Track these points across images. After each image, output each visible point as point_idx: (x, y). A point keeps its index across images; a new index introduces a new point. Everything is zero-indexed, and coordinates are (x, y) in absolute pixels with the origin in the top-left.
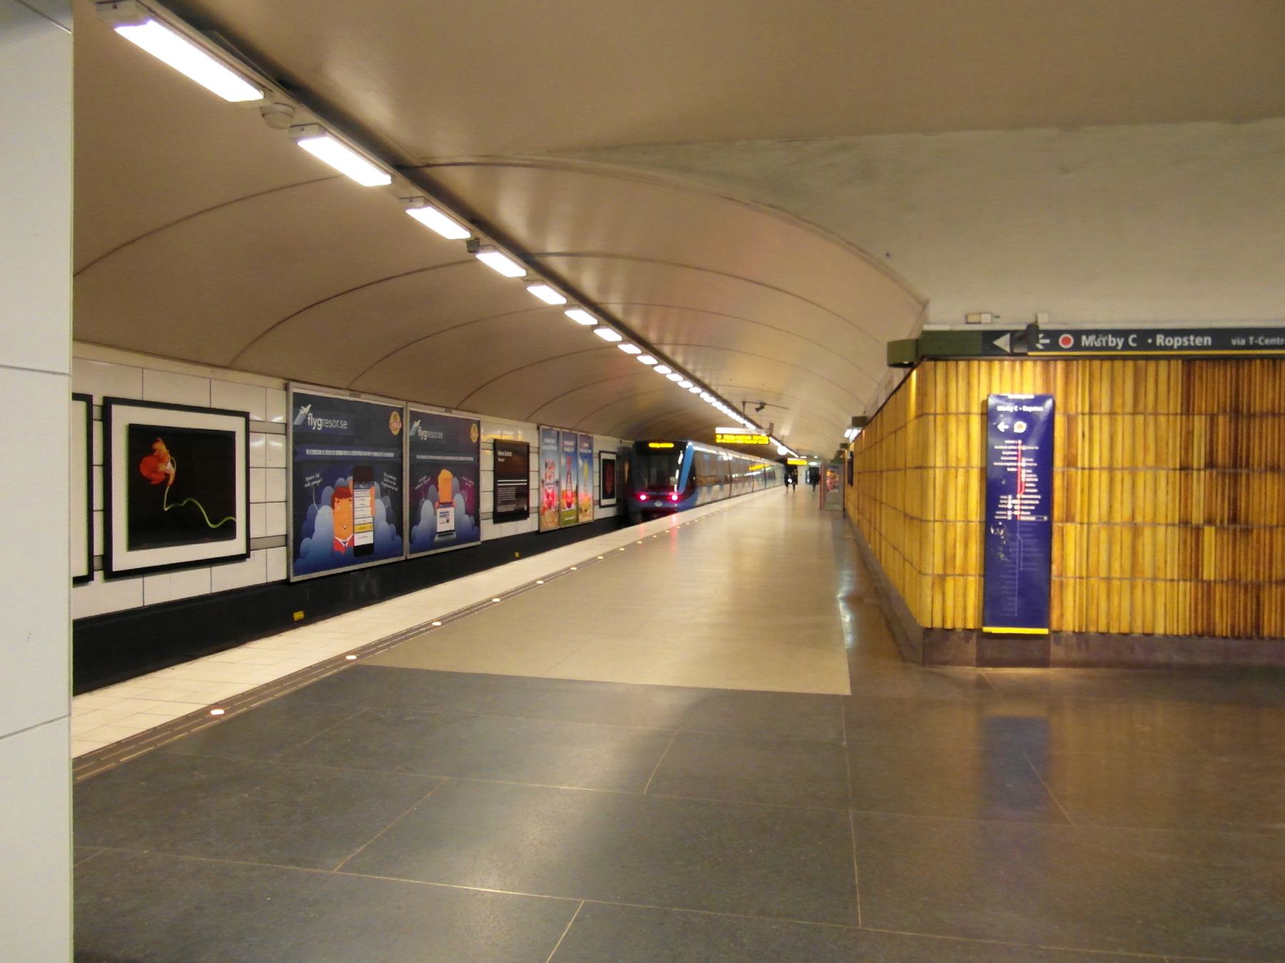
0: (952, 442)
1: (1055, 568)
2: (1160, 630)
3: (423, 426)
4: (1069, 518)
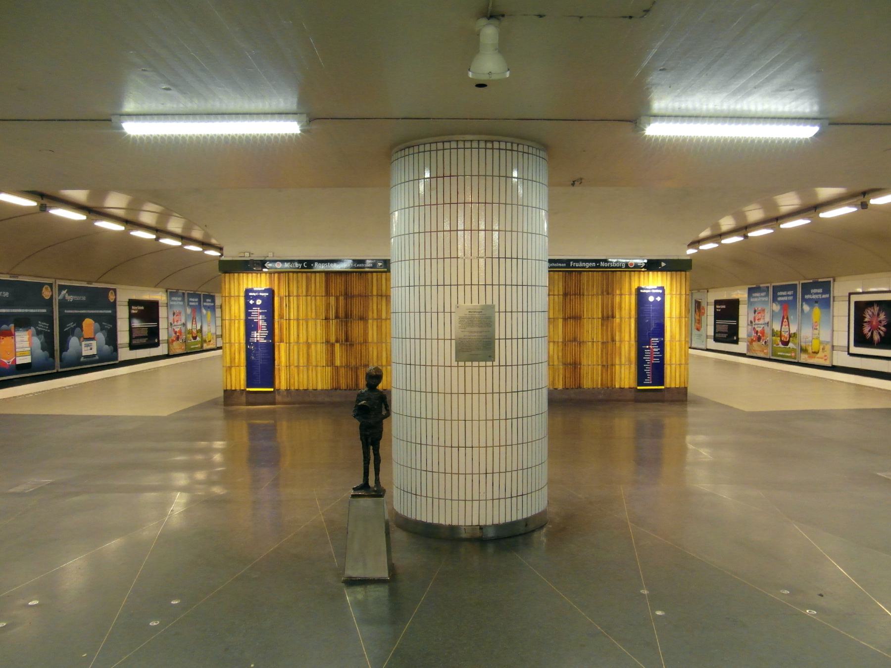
0: (233, 308)
1: (276, 362)
2: (319, 388)
3: (69, 293)
4: (281, 341)
